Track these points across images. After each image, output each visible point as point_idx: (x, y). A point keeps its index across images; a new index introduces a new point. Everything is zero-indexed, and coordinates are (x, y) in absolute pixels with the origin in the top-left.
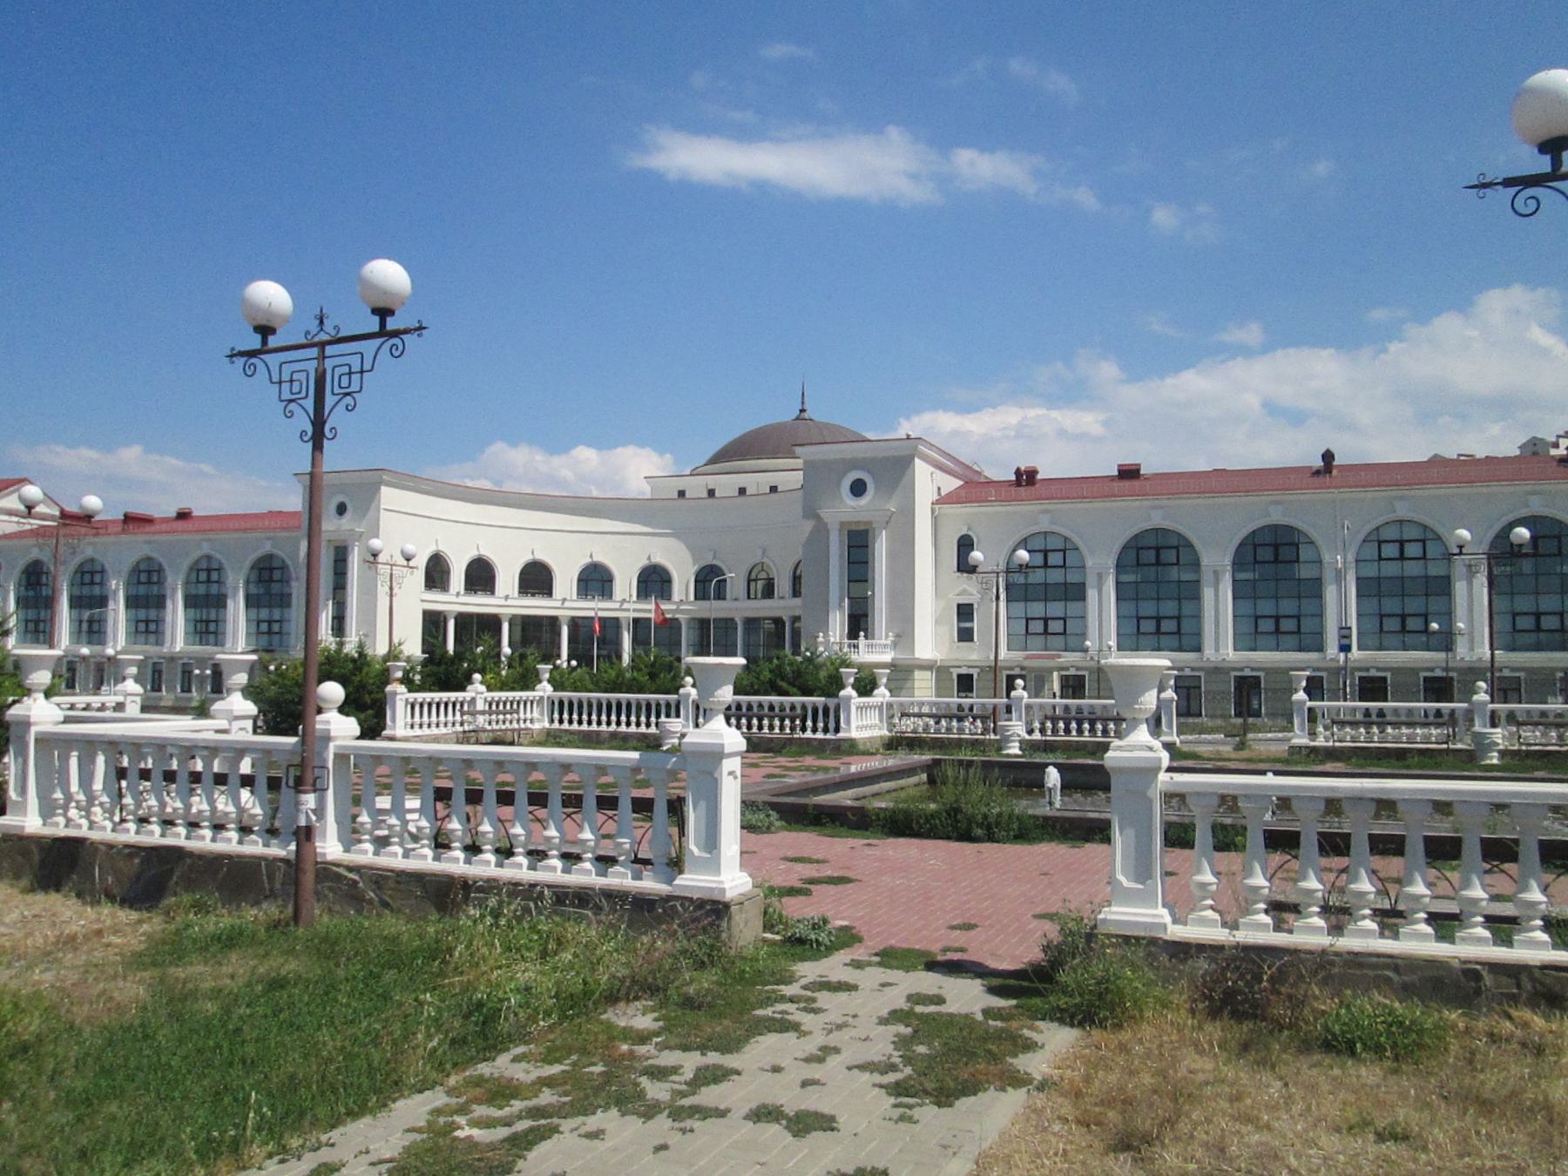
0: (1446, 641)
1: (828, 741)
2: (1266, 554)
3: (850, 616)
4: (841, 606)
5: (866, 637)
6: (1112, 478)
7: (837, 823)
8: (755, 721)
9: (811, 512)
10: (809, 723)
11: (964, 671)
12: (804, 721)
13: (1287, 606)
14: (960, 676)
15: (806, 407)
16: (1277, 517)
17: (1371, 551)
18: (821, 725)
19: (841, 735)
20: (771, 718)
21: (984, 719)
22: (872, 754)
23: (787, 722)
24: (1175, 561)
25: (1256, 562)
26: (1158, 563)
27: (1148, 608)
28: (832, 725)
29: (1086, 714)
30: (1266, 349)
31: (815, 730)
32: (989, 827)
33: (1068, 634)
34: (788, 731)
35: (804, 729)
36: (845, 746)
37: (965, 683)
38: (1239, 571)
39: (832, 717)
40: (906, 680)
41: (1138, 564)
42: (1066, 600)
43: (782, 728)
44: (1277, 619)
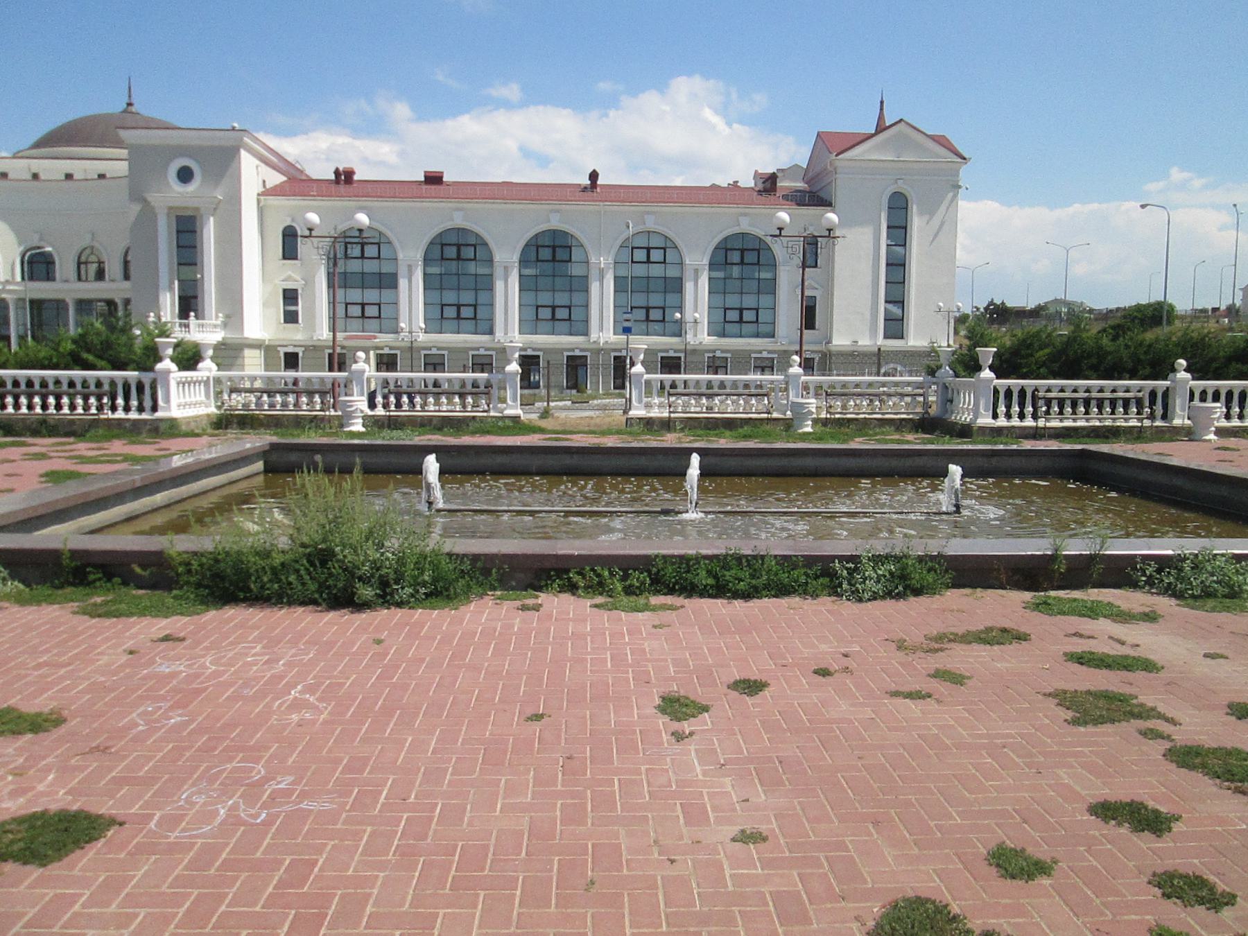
0: (679, 330)
1: (145, 421)
2: (546, 254)
3: (180, 298)
4: (171, 289)
5: (197, 317)
6: (419, 183)
7: (117, 580)
8: (51, 400)
9: (137, 195)
10: (120, 401)
11: (290, 349)
12: (113, 398)
13: (561, 299)
14: (286, 354)
15: (134, 101)
16: (555, 223)
17: (625, 256)
18: (134, 403)
19: (159, 414)
20: (30, 397)
21: (323, 394)
22: (198, 435)
23: (92, 400)
24: (473, 257)
25: (538, 260)
26: (459, 258)
27: (450, 297)
28: (148, 403)
29: (405, 387)
30: (524, 104)
31: (127, 409)
32: (384, 583)
33: (384, 318)
34: (94, 411)
35: (114, 408)
36: (163, 427)
37: (291, 361)
38: (526, 267)
39: (147, 394)
40: (236, 357)
41: (442, 259)
42: (380, 288)
43: (86, 407)
44: (554, 308)
